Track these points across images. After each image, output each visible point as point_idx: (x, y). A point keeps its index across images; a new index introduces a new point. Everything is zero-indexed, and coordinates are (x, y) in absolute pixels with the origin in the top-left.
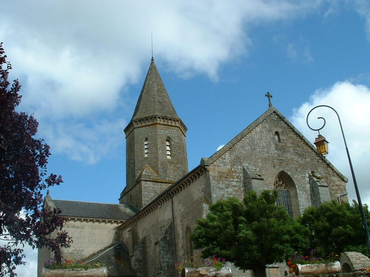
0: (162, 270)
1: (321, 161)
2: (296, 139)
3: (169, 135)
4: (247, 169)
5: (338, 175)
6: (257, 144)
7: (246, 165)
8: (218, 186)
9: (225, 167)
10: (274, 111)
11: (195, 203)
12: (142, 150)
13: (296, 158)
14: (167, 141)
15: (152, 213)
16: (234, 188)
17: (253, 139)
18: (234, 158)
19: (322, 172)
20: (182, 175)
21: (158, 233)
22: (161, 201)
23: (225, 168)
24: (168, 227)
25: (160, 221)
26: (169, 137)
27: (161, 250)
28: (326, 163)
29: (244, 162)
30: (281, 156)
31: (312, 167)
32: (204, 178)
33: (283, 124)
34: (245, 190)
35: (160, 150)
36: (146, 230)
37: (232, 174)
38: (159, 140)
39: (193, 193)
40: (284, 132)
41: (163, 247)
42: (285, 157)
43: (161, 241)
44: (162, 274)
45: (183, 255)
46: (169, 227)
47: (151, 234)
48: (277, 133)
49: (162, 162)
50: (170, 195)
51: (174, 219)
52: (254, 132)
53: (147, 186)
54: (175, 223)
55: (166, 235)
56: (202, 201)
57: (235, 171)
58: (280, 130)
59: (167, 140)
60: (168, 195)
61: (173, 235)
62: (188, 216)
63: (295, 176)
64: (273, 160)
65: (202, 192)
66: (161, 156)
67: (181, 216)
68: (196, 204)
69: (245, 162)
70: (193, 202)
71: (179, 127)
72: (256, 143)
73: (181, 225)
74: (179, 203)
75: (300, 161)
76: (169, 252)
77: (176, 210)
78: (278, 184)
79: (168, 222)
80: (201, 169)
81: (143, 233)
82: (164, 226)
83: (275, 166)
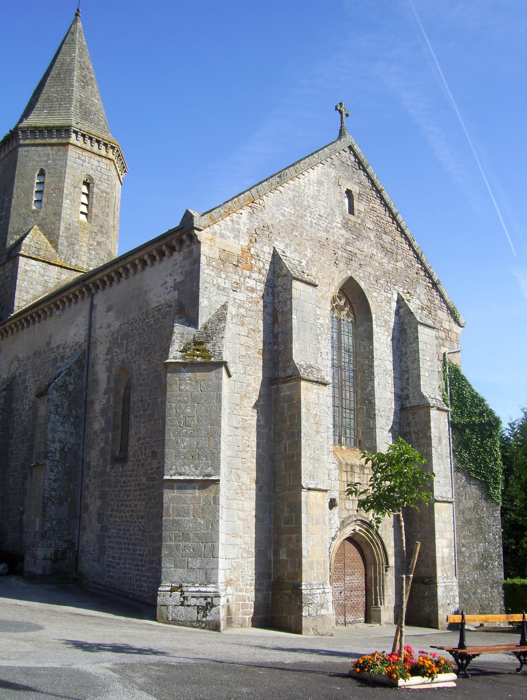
0: (49, 459)
1: (422, 273)
2: (383, 216)
3: (91, 173)
4: (283, 256)
5: (448, 308)
6: (309, 206)
7: (280, 247)
8: (215, 282)
9: (236, 241)
10: (350, 144)
11: (152, 315)
12: (28, 194)
13: (379, 255)
14: (85, 183)
15: (37, 325)
16: (250, 294)
17: (301, 193)
18: (257, 224)
19: (423, 297)
20: (105, 259)
21: (46, 371)
22: (65, 299)
23: (236, 246)
24: (73, 361)
25: (54, 345)
26: (90, 177)
27: (51, 413)
28: (432, 280)
29: (276, 239)
30: (351, 245)
31: (405, 282)
32: (184, 259)
33: (363, 178)
34: (274, 303)
35: (68, 199)
36: (19, 361)
37: (250, 260)
38: (68, 178)
39: (150, 291)
40: (363, 196)
41: (56, 405)
42: (358, 247)
43: (54, 392)
44: (48, 467)
45: (103, 430)
46: (76, 362)
47: (30, 373)
48: (349, 193)
49: (67, 226)
50: (89, 290)
51: (91, 344)
52: (306, 179)
53: (29, 268)
54: (92, 355)
55: (67, 378)
56: (170, 311)
57: (257, 256)
58: (356, 190)
59: (84, 182)
60: (84, 289)
61: (84, 381)
62: (127, 343)
63: (373, 294)
64: (336, 250)
65: (174, 290)
66: (69, 212)
67: (110, 341)
68: (152, 317)
69: (279, 239)
70: (147, 311)
71: (113, 161)
72: (306, 203)
73: (107, 360)
74: (109, 309)
75: (386, 265)
76: (69, 419)
77: (98, 326)
78: (336, 303)
79: (75, 350)
80: (181, 235)
81: (10, 366)
82: (63, 358)
83: (337, 263)
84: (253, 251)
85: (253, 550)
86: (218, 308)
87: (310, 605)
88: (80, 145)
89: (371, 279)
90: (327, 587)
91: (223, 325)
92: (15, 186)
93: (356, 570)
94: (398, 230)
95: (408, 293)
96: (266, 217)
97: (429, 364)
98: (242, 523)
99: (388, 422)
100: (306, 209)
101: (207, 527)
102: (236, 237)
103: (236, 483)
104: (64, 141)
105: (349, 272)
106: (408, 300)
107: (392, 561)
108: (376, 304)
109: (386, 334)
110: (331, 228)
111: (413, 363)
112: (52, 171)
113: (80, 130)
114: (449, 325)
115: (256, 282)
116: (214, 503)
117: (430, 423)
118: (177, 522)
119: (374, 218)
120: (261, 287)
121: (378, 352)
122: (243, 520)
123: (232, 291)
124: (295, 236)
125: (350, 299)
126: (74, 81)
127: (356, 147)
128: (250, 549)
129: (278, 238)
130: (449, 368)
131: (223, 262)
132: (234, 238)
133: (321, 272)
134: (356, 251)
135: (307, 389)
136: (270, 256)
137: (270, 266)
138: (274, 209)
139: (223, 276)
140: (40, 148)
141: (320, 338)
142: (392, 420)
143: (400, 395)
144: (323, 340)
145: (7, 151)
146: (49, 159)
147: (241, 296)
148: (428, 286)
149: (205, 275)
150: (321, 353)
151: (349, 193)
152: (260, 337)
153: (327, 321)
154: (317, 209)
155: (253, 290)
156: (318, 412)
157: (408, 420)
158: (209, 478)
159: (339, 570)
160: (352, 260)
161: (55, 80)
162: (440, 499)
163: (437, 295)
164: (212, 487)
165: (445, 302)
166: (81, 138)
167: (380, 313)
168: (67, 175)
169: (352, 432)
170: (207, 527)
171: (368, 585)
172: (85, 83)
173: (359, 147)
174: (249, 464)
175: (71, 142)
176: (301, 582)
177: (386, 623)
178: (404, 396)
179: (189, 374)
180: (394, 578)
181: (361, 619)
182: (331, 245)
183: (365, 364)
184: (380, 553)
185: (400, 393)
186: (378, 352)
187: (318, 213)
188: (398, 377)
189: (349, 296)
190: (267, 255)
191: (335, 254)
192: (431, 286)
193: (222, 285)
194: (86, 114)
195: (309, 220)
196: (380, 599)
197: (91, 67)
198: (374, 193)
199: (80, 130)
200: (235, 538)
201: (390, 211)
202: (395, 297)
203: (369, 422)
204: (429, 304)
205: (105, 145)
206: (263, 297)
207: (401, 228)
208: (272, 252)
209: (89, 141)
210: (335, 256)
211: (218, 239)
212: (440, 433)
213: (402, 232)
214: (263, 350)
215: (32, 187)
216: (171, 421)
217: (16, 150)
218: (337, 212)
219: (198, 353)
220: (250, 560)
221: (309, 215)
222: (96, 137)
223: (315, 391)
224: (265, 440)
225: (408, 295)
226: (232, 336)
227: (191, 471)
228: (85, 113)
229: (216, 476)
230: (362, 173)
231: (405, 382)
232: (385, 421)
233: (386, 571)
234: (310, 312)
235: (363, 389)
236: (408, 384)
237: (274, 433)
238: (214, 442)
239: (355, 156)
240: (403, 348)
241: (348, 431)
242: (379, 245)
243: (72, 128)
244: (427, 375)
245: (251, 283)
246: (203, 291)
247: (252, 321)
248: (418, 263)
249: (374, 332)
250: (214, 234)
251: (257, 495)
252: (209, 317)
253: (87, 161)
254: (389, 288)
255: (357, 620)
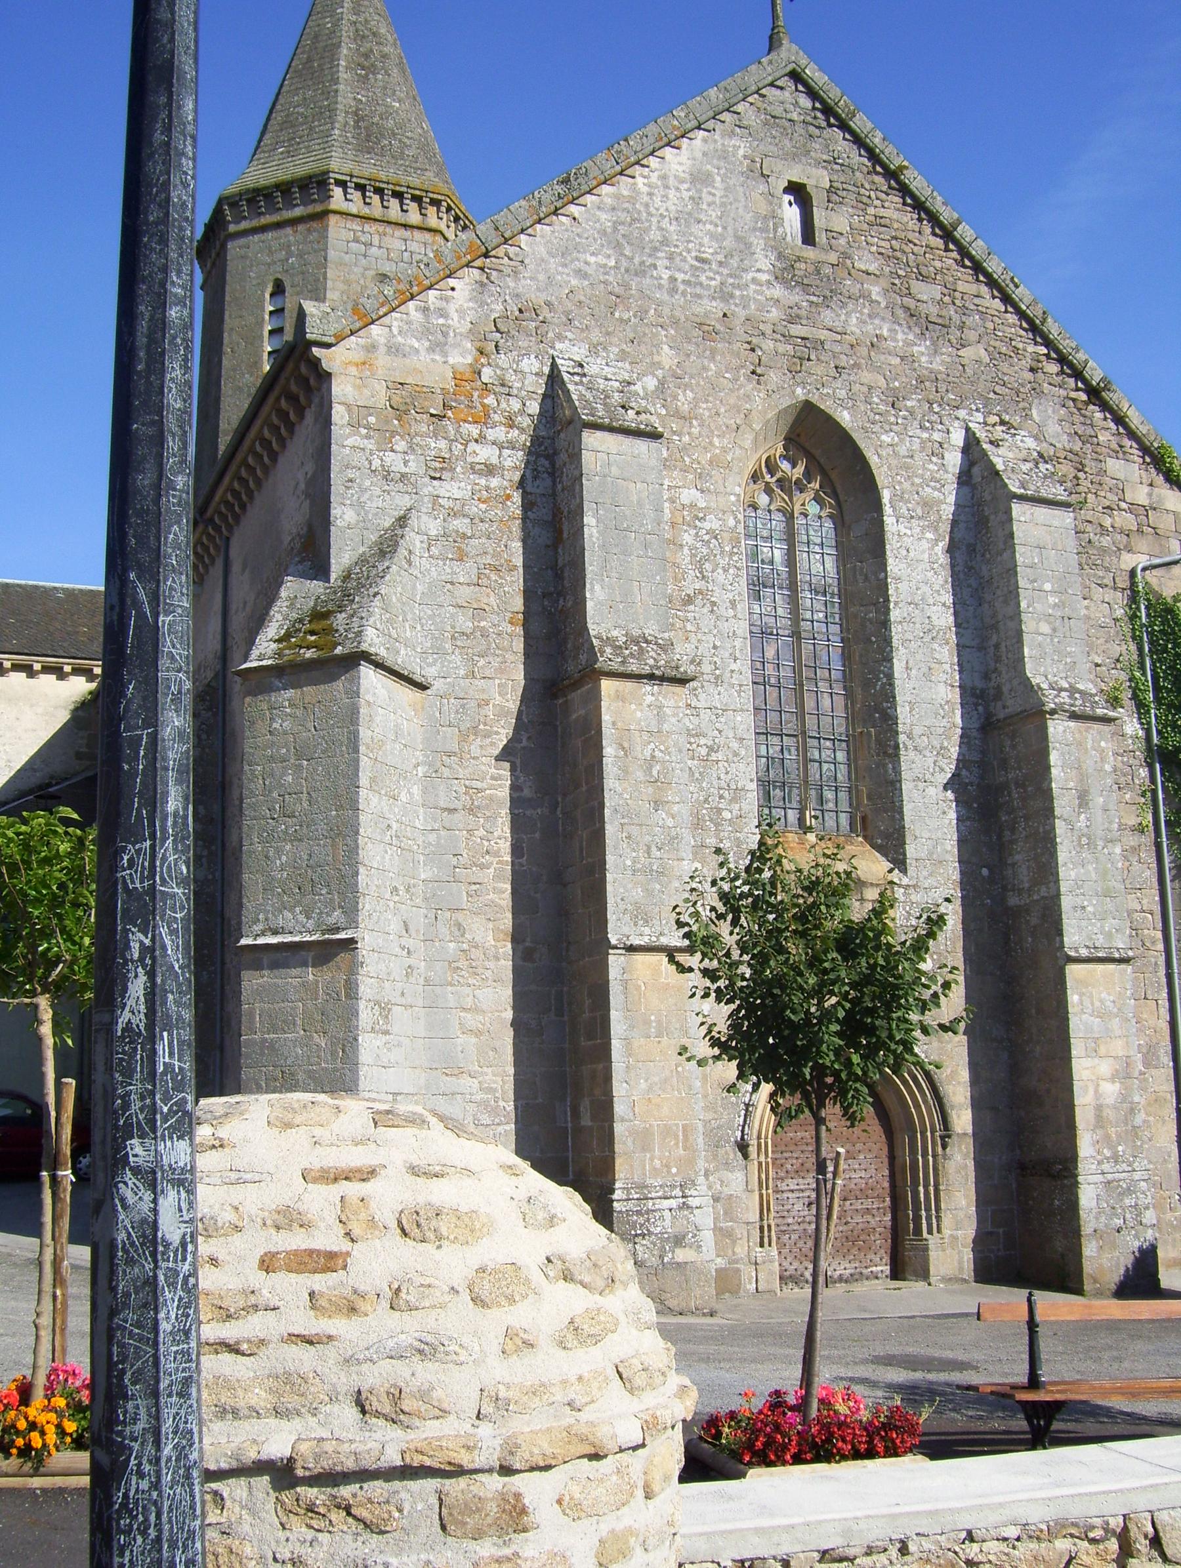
1: (1053, 368)
5: (1145, 450)
6: (665, 242)
7: (569, 352)
8: (376, 463)
9: (437, 357)
13: (901, 337)
16: (483, 482)
17: (639, 212)
23: (436, 368)
28: (1084, 381)
29: (560, 337)
30: (804, 322)
31: (992, 395)
57: (503, 385)
58: (817, 179)
64: (755, 340)
72: (655, 235)
75: (924, 359)
78: (779, 475)
84: (487, 374)
85: (510, 1107)
86: (387, 525)
87: (637, 1240)
88: (354, 211)
89: (876, 400)
90: (694, 1193)
91: (387, 564)
92: (226, 327)
93: (859, 1146)
94: (964, 266)
95: (1003, 423)
96: (528, 287)
97: (1052, 600)
98: (474, 1040)
99: (943, 763)
100: (656, 249)
101: (334, 1054)
102: (438, 346)
103: (452, 945)
104: (319, 208)
105: (799, 391)
106: (991, 442)
107: (963, 1120)
108: (894, 462)
109: (929, 535)
110: (739, 287)
111: (1006, 602)
112: (298, 279)
113: (351, 176)
114: (1150, 495)
115: (502, 450)
116: (348, 996)
117: (1048, 755)
118: (272, 1046)
119: (883, 244)
120: (514, 460)
121: (903, 587)
122: (478, 1033)
123: (427, 479)
124: (621, 320)
125: (822, 461)
126: (341, 69)
127: (812, 72)
128: (501, 1103)
129: (569, 334)
130: (1147, 607)
131: (400, 412)
132: (431, 350)
133: (707, 401)
134: (823, 335)
135: (619, 697)
136: (542, 381)
137: (541, 405)
138: (553, 263)
139: (401, 445)
140: (270, 235)
141: (707, 566)
142: (955, 756)
143: (983, 691)
144: (720, 571)
145: (213, 255)
146: (290, 254)
147: (454, 489)
148: (1074, 400)
149: (347, 451)
150: (714, 604)
151: (797, 190)
152: (514, 583)
153: (731, 522)
154: (691, 245)
155: (490, 470)
156: (657, 753)
157: (1002, 752)
158: (334, 937)
159: (804, 1147)
160: (809, 360)
161: (300, 76)
162: (1084, 952)
163: (1105, 419)
164: (343, 957)
165: (1132, 435)
166: (356, 195)
167: (907, 485)
168: (329, 284)
169: (843, 795)
170: (334, 1054)
171: (899, 1183)
172: (367, 67)
173: (821, 69)
174: (492, 896)
175: (333, 207)
176: (613, 1181)
177: (948, 1280)
178: (992, 692)
179: (290, 693)
180: (971, 1164)
181: (879, 1268)
182: (739, 330)
183: (870, 620)
184: (925, 1101)
185: (979, 684)
186: (903, 587)
187: (694, 254)
188: (974, 643)
189: (817, 453)
190: (531, 379)
191: (753, 350)
192: (1084, 397)
193: (399, 467)
194: (369, 137)
195: (665, 277)
196: (929, 1218)
197: (383, 31)
198: (878, 179)
199: (351, 176)
200: (454, 1078)
201: (934, 219)
202: (958, 437)
203: (885, 765)
204: (1077, 446)
205: (417, 199)
206: (522, 484)
207: (971, 258)
208: (546, 370)
209: (376, 198)
210: (753, 357)
211: (382, 360)
212: (1082, 777)
213: (978, 268)
214: (527, 613)
215: (261, 323)
216: (253, 807)
217: (223, 246)
218: (758, 243)
219: (313, 638)
220: (500, 1129)
221: (667, 263)
222: (391, 186)
223: (649, 699)
224: (537, 835)
225: (999, 428)
226: (430, 588)
227: (297, 922)
228: (368, 136)
229: (350, 932)
230: (838, 133)
231: (992, 654)
232: (930, 761)
233: (944, 1147)
234: (640, 504)
235: (867, 684)
236: (998, 659)
237: (563, 814)
238: (345, 848)
239: (812, 94)
240: (984, 568)
241: (829, 795)
242: (900, 312)
243: (331, 175)
244: (1045, 628)
245: (485, 453)
246: (342, 489)
247: (490, 546)
248: (1036, 344)
249: (888, 536)
250: (372, 348)
251: (516, 970)
252: (361, 550)
253: (376, 242)
254: (935, 418)
255: (864, 1271)
